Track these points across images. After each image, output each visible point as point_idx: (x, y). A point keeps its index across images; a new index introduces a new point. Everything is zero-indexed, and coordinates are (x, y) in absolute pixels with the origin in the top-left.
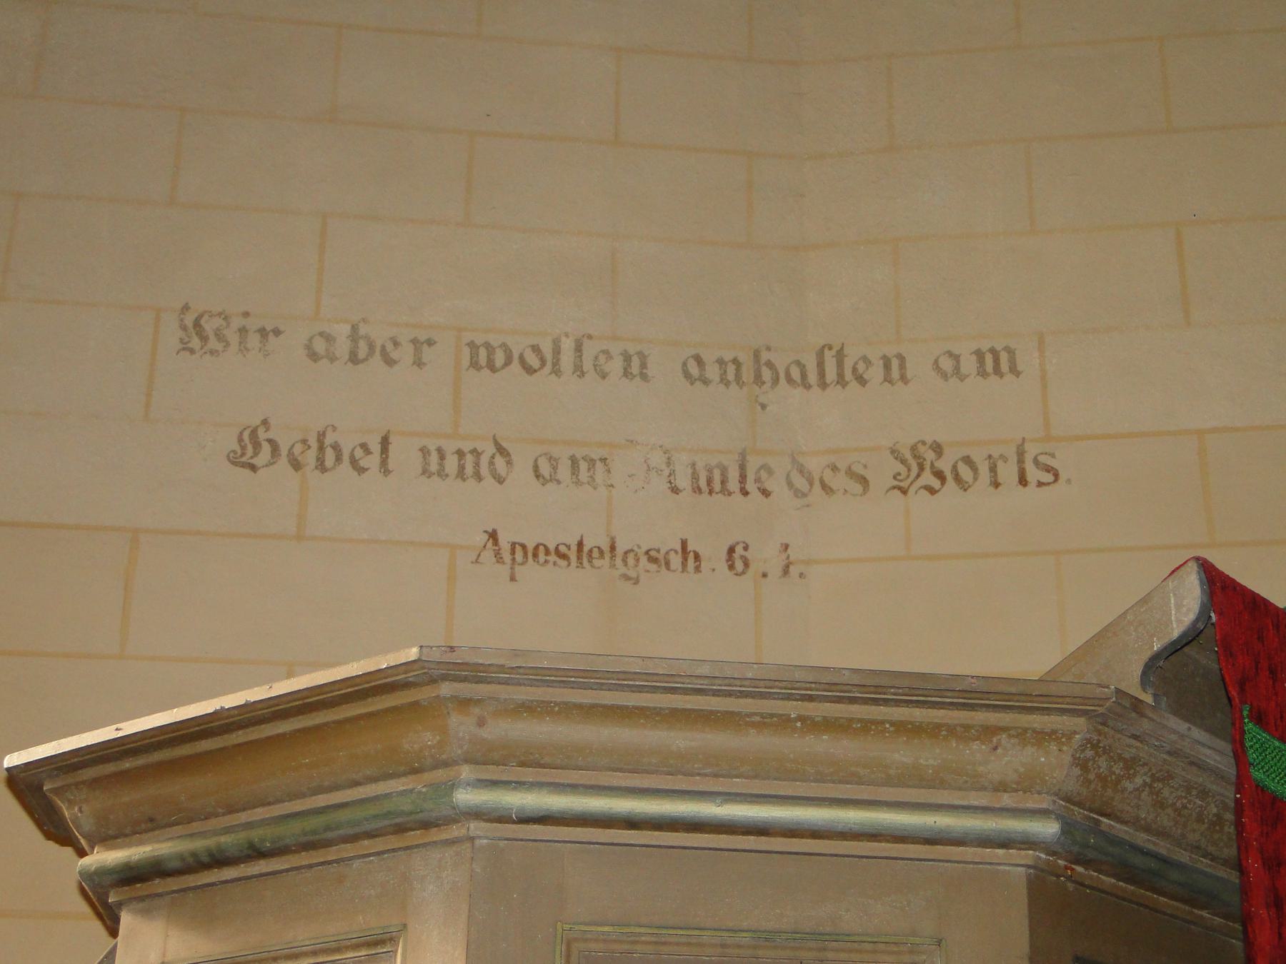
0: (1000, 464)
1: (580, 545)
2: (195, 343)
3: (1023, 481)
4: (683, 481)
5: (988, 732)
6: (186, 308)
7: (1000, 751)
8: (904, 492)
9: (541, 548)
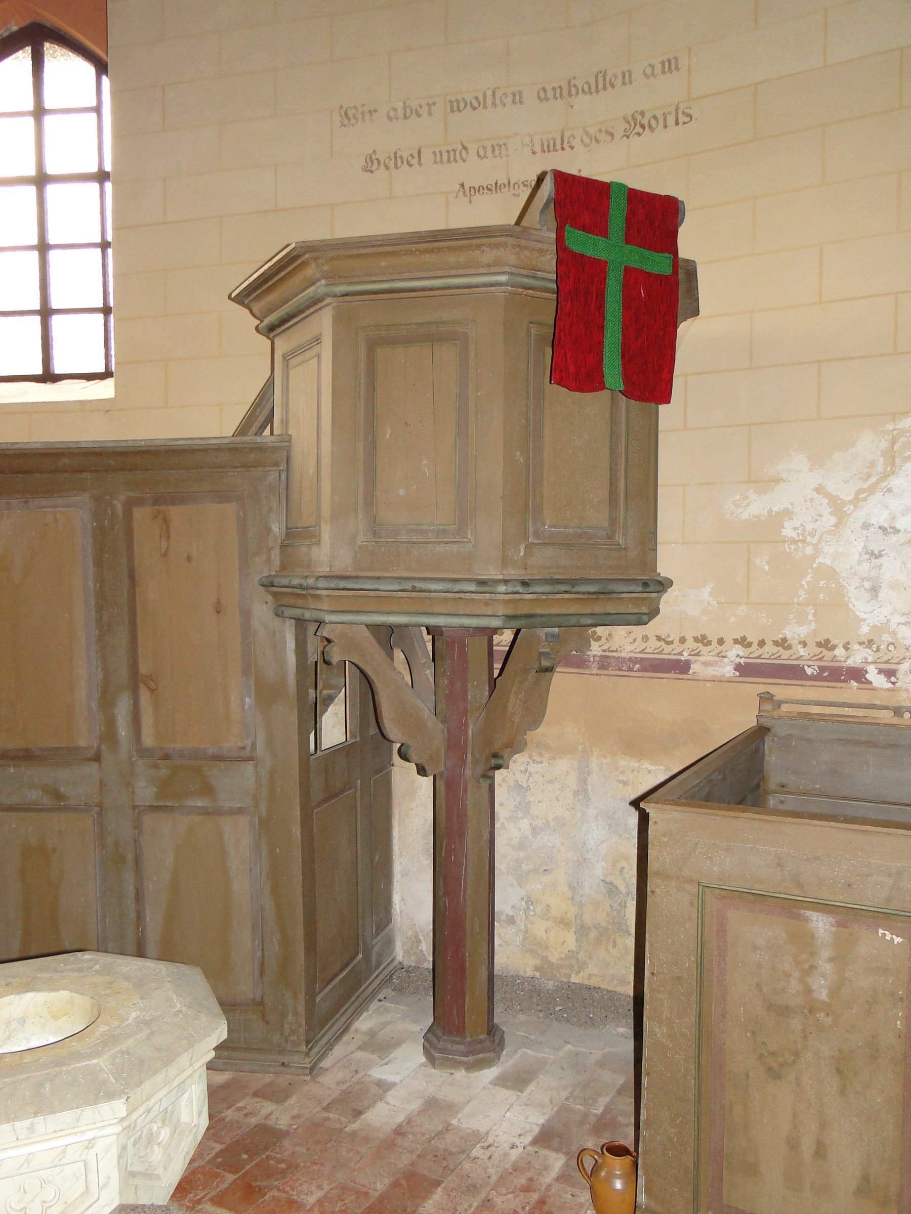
0: (668, 116)
1: (496, 183)
2: (346, 121)
3: (677, 123)
4: (538, 149)
5: (479, 247)
6: (341, 107)
7: (485, 253)
8: (628, 137)
9: (481, 188)
